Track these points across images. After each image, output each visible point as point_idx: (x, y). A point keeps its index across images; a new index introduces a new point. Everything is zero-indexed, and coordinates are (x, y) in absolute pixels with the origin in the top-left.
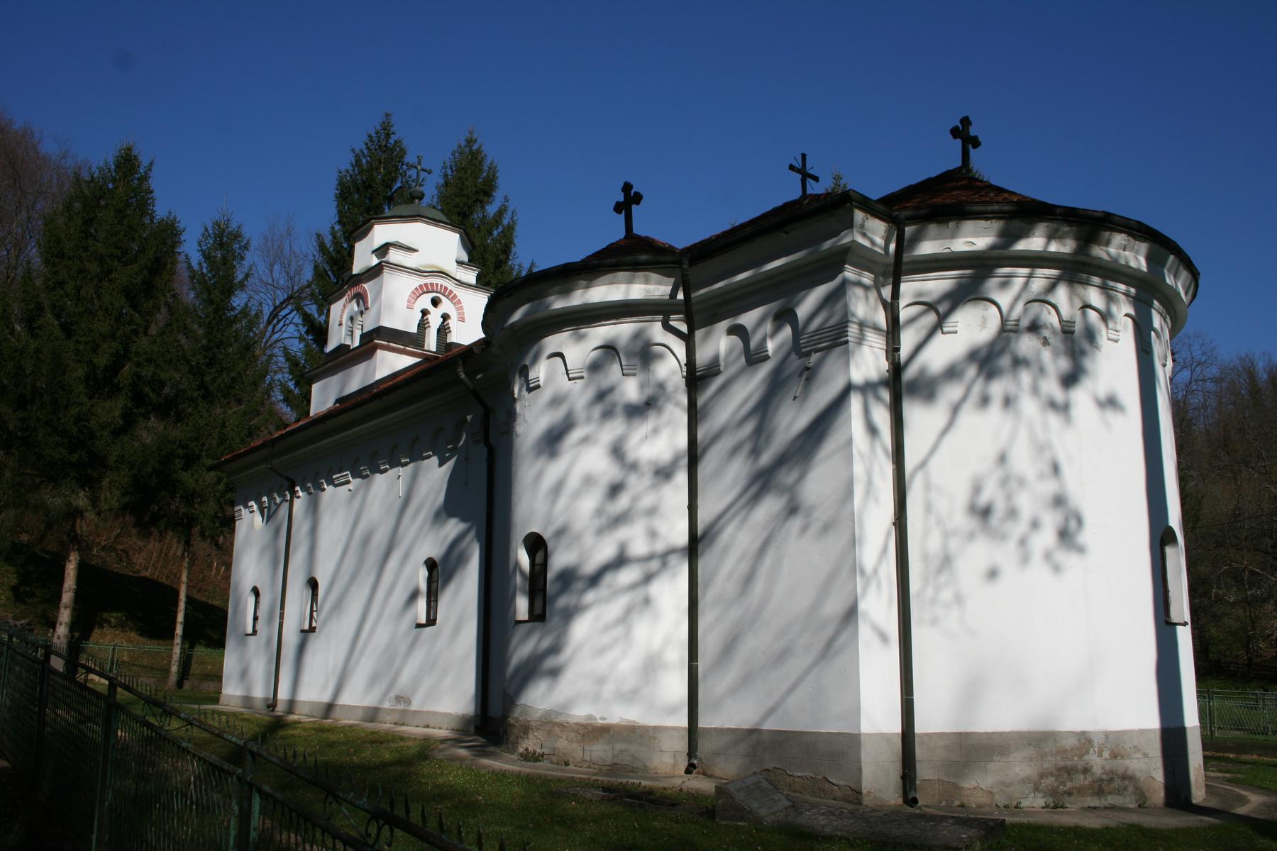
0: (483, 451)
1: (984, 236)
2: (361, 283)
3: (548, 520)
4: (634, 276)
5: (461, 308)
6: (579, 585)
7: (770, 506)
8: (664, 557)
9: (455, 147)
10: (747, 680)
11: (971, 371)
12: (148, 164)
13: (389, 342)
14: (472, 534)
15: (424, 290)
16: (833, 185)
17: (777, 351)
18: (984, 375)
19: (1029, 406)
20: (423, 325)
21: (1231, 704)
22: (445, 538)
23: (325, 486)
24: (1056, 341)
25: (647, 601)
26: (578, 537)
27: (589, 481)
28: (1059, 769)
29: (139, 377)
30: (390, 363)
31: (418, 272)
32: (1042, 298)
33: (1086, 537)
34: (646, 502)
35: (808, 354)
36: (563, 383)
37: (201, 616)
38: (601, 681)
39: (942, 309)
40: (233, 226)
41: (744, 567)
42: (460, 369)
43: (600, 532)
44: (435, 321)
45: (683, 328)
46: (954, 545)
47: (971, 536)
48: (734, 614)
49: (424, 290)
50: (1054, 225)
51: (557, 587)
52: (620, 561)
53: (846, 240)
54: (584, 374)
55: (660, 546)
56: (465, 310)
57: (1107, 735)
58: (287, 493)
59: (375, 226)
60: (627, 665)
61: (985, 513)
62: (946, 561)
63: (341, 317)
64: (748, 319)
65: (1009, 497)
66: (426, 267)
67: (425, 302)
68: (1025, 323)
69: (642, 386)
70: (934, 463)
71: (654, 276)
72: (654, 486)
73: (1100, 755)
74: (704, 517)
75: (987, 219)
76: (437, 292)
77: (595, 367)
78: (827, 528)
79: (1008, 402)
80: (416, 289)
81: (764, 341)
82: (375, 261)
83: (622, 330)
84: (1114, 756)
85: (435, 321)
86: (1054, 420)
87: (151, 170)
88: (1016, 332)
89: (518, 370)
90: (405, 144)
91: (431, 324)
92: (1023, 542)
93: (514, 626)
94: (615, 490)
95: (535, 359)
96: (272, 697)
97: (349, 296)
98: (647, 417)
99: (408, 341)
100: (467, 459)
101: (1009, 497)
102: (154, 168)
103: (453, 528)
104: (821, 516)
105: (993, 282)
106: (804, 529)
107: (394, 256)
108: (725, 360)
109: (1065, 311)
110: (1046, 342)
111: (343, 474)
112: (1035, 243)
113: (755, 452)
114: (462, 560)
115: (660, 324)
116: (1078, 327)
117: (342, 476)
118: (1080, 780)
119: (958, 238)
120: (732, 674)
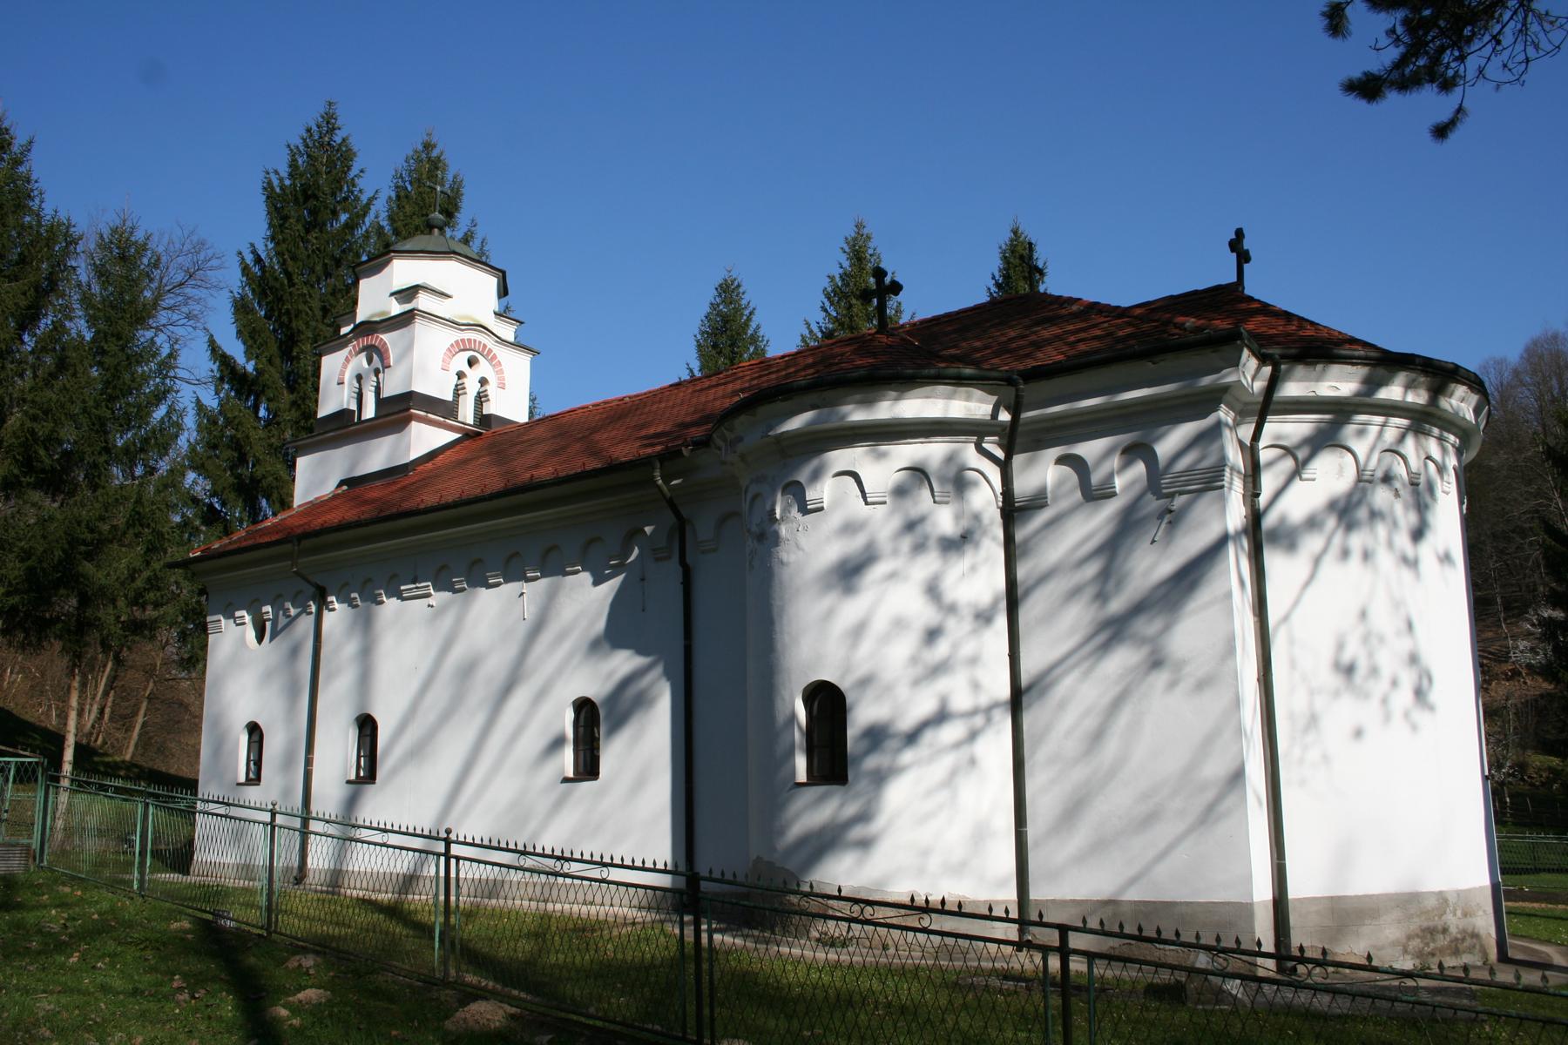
0: (673, 569)
1: (1347, 381)
2: (377, 332)
3: (847, 669)
4: (955, 392)
5: (501, 372)
6: (891, 744)
7: (1122, 659)
8: (988, 711)
9: (411, 153)
10: (1099, 847)
11: (1331, 522)
12: (25, 142)
13: (427, 412)
14: (659, 670)
15: (461, 346)
16: (853, 235)
17: (1126, 488)
18: (1343, 526)
19: (1385, 559)
20: (458, 391)
21: (53, 722)
22: (610, 675)
23: (385, 599)
24: (1406, 493)
25: (973, 762)
26: (889, 689)
27: (899, 624)
28: (1423, 930)
29: (33, 432)
30: (424, 438)
31: (454, 324)
32: (1394, 448)
33: (1434, 696)
34: (967, 649)
35: (1171, 496)
36: (857, 506)
37: (53, 748)
38: (925, 853)
39: (1301, 455)
40: (139, 236)
41: (1090, 723)
42: (657, 473)
43: (916, 682)
44: (472, 387)
45: (1000, 454)
46: (1320, 703)
47: (1336, 694)
48: (1079, 774)
49: (461, 346)
50: (1413, 375)
51: (864, 744)
52: (941, 717)
53: (1231, 379)
54: (887, 499)
55: (984, 700)
56: (506, 375)
57: (1459, 893)
58: (311, 603)
59: (394, 261)
60: (951, 835)
61: (1349, 670)
62: (1313, 720)
63: (342, 373)
64: (1089, 449)
65: (1370, 655)
66: (461, 317)
67: (460, 362)
68: (1379, 474)
69: (958, 517)
70: (1295, 617)
71: (978, 393)
72: (974, 631)
73: (1455, 915)
74: (1028, 669)
75: (1353, 364)
76: (474, 351)
77: (900, 492)
78: (1202, 685)
79: (1367, 556)
80: (452, 345)
81: (1111, 476)
82: (396, 308)
83: (933, 451)
84: (1465, 915)
85: (472, 387)
86: (1406, 574)
87: (29, 150)
88: (1370, 482)
89: (781, 486)
90: (355, 144)
91: (467, 390)
92: (1385, 701)
93: (791, 789)
94: (932, 635)
95: (816, 476)
96: (296, 865)
97: (354, 346)
98: (964, 553)
99: (443, 410)
100: (643, 580)
101: (1370, 655)
102: (35, 148)
103: (624, 662)
104: (1194, 671)
105: (1350, 429)
106: (1172, 685)
107: (423, 302)
108: (1053, 491)
109: (1415, 463)
110: (1397, 494)
111: (418, 585)
112: (1393, 392)
113: (1102, 597)
114: (642, 701)
115: (973, 445)
116: (1422, 480)
117: (417, 588)
118: (1442, 941)
119: (1323, 381)
120: (1080, 837)
